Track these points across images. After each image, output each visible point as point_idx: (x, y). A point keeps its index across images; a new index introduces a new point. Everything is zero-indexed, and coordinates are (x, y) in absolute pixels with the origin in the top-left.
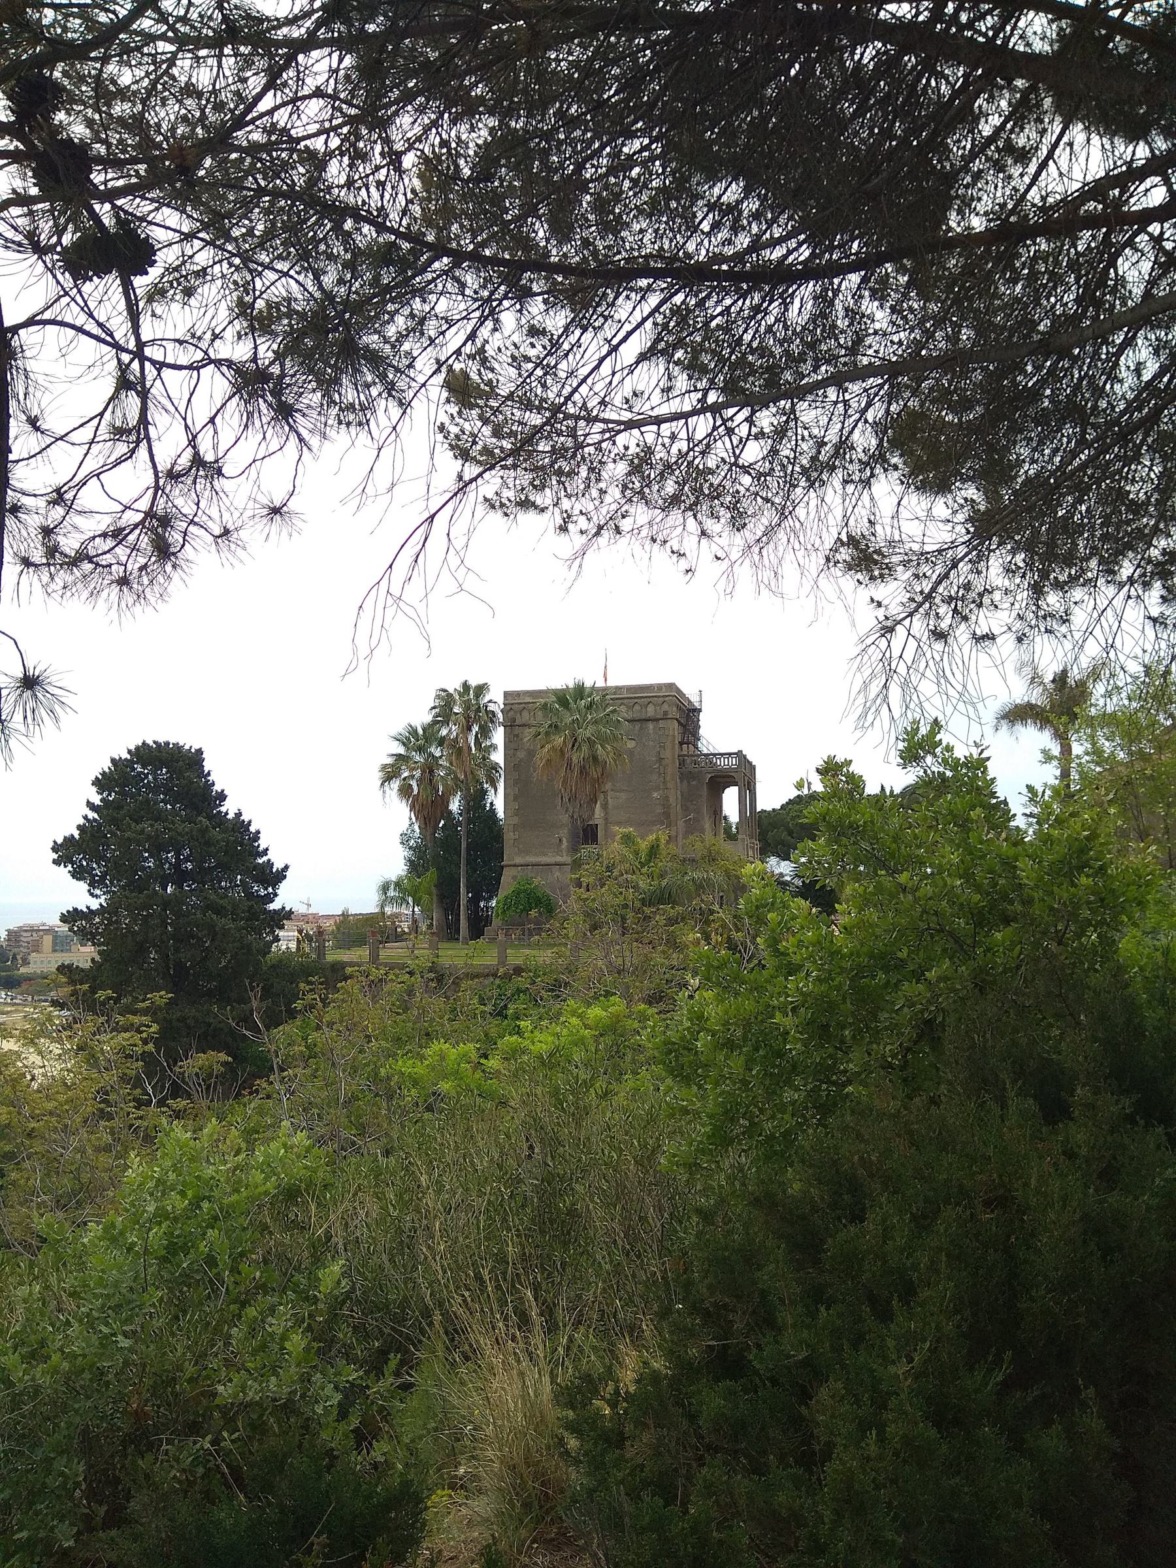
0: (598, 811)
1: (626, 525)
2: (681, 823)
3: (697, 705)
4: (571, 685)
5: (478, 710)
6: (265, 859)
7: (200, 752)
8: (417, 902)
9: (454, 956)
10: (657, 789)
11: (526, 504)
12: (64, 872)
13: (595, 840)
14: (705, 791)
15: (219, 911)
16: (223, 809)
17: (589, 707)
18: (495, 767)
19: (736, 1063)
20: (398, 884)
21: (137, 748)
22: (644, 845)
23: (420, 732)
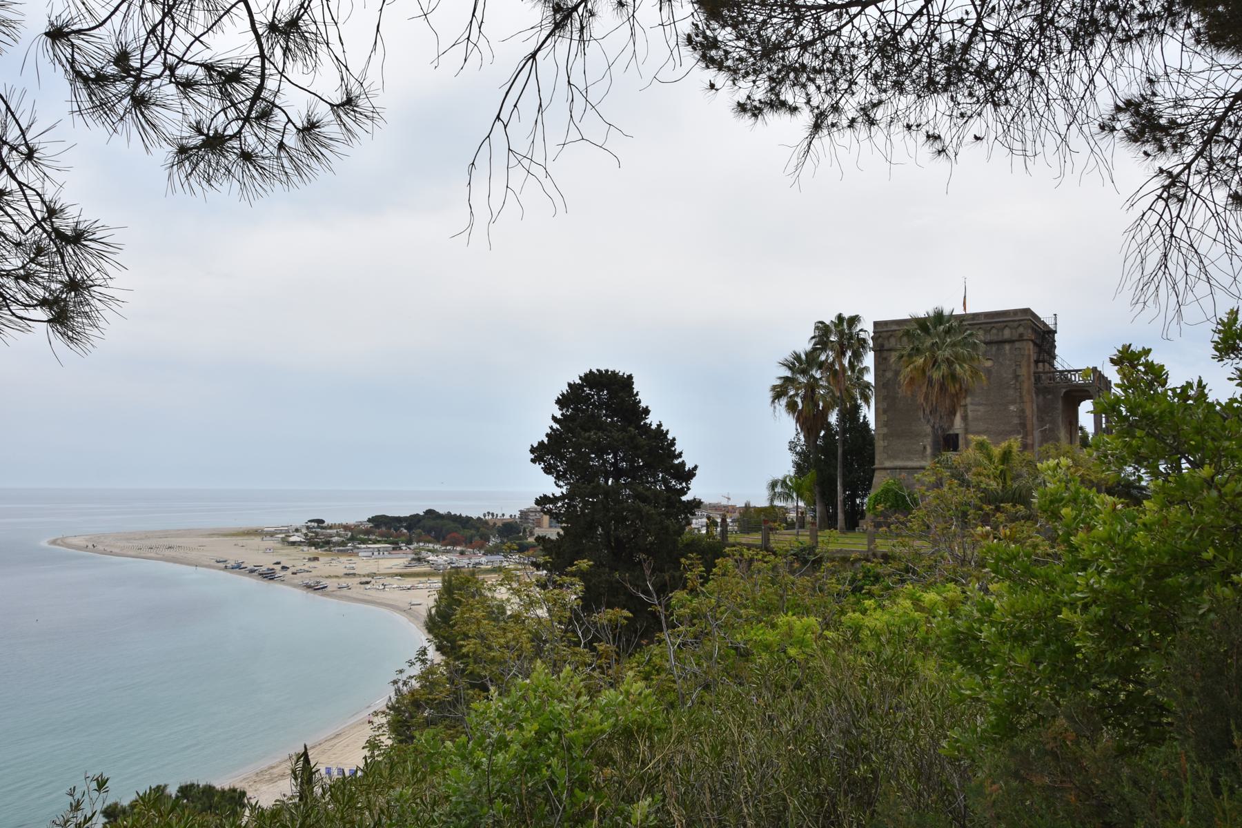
0: (958, 421)
1: (879, 114)
2: (1037, 434)
3: (1052, 327)
4: (932, 314)
5: (851, 337)
6: (680, 460)
7: (630, 377)
8: (800, 496)
9: (835, 542)
10: (1013, 402)
11: (778, 104)
12: (538, 467)
13: (956, 448)
14: (1060, 405)
15: (645, 500)
16: (648, 421)
17: (948, 332)
18: (868, 385)
19: (1022, 658)
20: (784, 482)
21: (586, 375)
22: (997, 451)
23: (803, 357)
